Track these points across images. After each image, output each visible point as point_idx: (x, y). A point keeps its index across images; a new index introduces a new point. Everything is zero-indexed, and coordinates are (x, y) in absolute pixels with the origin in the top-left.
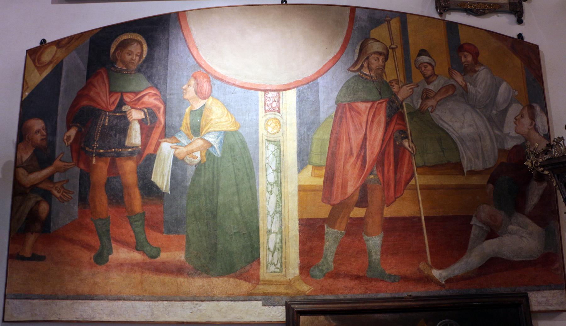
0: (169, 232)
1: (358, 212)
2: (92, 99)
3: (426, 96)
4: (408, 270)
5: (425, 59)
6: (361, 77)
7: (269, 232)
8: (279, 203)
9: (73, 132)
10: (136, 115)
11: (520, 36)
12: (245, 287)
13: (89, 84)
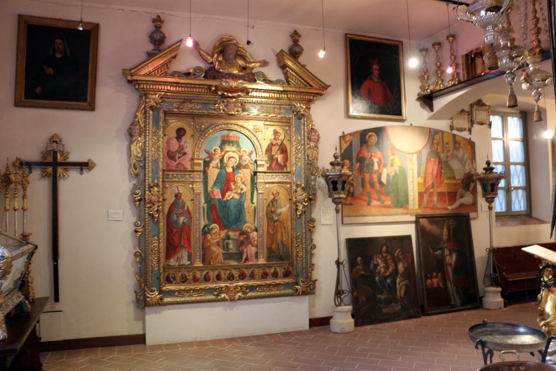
0: (387, 196)
1: (431, 190)
2: (363, 154)
3: (447, 157)
4: (443, 207)
5: (447, 145)
6: (432, 151)
7: (411, 196)
8: (413, 187)
9: (358, 165)
10: (376, 160)
11: (470, 139)
12: (406, 211)
13: (361, 150)
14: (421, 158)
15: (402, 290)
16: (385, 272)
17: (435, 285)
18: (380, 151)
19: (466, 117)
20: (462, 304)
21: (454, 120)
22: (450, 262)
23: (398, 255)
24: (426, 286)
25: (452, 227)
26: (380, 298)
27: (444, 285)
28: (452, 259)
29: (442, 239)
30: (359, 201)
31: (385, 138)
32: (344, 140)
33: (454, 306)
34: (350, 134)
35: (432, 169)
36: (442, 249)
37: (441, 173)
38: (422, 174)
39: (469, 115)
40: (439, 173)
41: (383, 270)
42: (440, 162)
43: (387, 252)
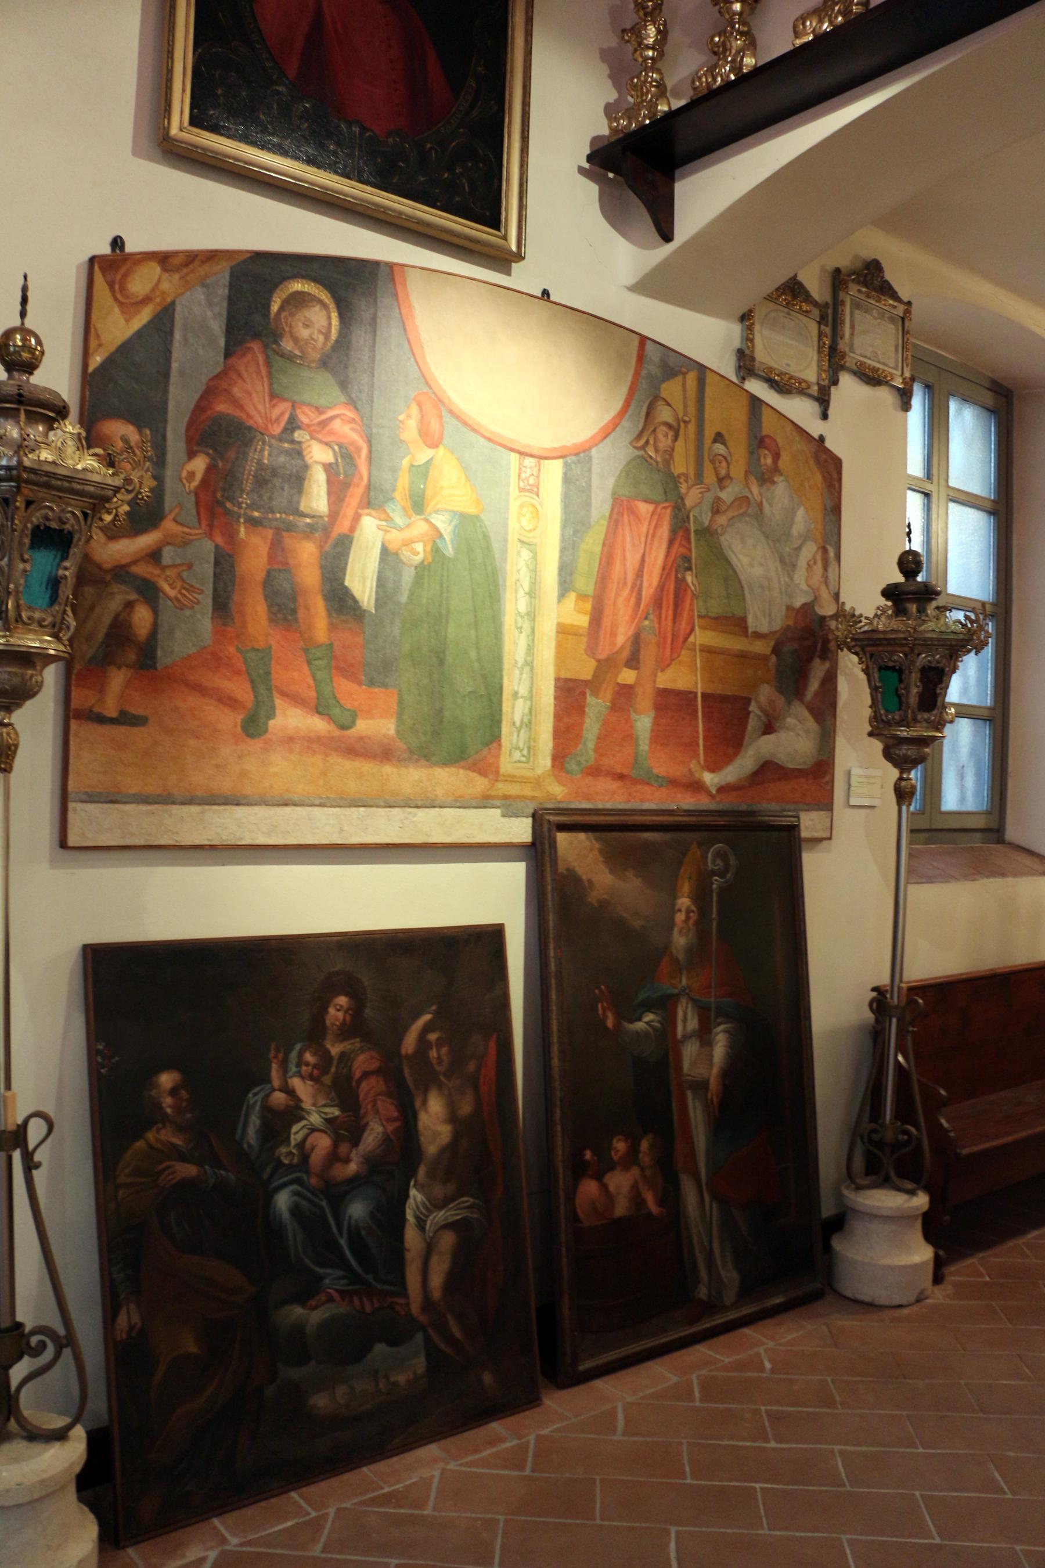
0: (371, 683)
1: (627, 676)
2: (236, 403)
4: (678, 771)
5: (719, 448)
6: (645, 460)
8: (530, 649)
9: (199, 464)
10: (318, 454)
12: (480, 784)
14: (586, 491)
15: (434, 1259)
16: (334, 1157)
17: (621, 1209)
18: (352, 403)
19: (813, 328)
20: (748, 1290)
21: (757, 327)
22: (701, 1072)
23: (423, 1042)
24: (574, 1218)
25: (717, 882)
26: (299, 1328)
27: (661, 1202)
28: (711, 1056)
29: (667, 947)
30: (190, 701)
31: (389, 331)
32: (119, 289)
33: (711, 1308)
34: (163, 259)
35: (638, 557)
36: (665, 1005)
37: (681, 584)
38: (586, 583)
39: (822, 320)
40: (671, 586)
41: (323, 1143)
42: (680, 527)
43: (350, 1030)
